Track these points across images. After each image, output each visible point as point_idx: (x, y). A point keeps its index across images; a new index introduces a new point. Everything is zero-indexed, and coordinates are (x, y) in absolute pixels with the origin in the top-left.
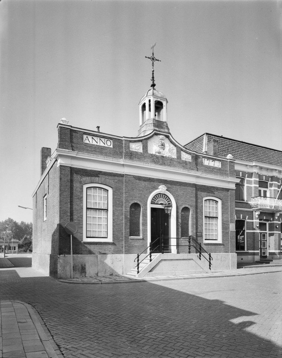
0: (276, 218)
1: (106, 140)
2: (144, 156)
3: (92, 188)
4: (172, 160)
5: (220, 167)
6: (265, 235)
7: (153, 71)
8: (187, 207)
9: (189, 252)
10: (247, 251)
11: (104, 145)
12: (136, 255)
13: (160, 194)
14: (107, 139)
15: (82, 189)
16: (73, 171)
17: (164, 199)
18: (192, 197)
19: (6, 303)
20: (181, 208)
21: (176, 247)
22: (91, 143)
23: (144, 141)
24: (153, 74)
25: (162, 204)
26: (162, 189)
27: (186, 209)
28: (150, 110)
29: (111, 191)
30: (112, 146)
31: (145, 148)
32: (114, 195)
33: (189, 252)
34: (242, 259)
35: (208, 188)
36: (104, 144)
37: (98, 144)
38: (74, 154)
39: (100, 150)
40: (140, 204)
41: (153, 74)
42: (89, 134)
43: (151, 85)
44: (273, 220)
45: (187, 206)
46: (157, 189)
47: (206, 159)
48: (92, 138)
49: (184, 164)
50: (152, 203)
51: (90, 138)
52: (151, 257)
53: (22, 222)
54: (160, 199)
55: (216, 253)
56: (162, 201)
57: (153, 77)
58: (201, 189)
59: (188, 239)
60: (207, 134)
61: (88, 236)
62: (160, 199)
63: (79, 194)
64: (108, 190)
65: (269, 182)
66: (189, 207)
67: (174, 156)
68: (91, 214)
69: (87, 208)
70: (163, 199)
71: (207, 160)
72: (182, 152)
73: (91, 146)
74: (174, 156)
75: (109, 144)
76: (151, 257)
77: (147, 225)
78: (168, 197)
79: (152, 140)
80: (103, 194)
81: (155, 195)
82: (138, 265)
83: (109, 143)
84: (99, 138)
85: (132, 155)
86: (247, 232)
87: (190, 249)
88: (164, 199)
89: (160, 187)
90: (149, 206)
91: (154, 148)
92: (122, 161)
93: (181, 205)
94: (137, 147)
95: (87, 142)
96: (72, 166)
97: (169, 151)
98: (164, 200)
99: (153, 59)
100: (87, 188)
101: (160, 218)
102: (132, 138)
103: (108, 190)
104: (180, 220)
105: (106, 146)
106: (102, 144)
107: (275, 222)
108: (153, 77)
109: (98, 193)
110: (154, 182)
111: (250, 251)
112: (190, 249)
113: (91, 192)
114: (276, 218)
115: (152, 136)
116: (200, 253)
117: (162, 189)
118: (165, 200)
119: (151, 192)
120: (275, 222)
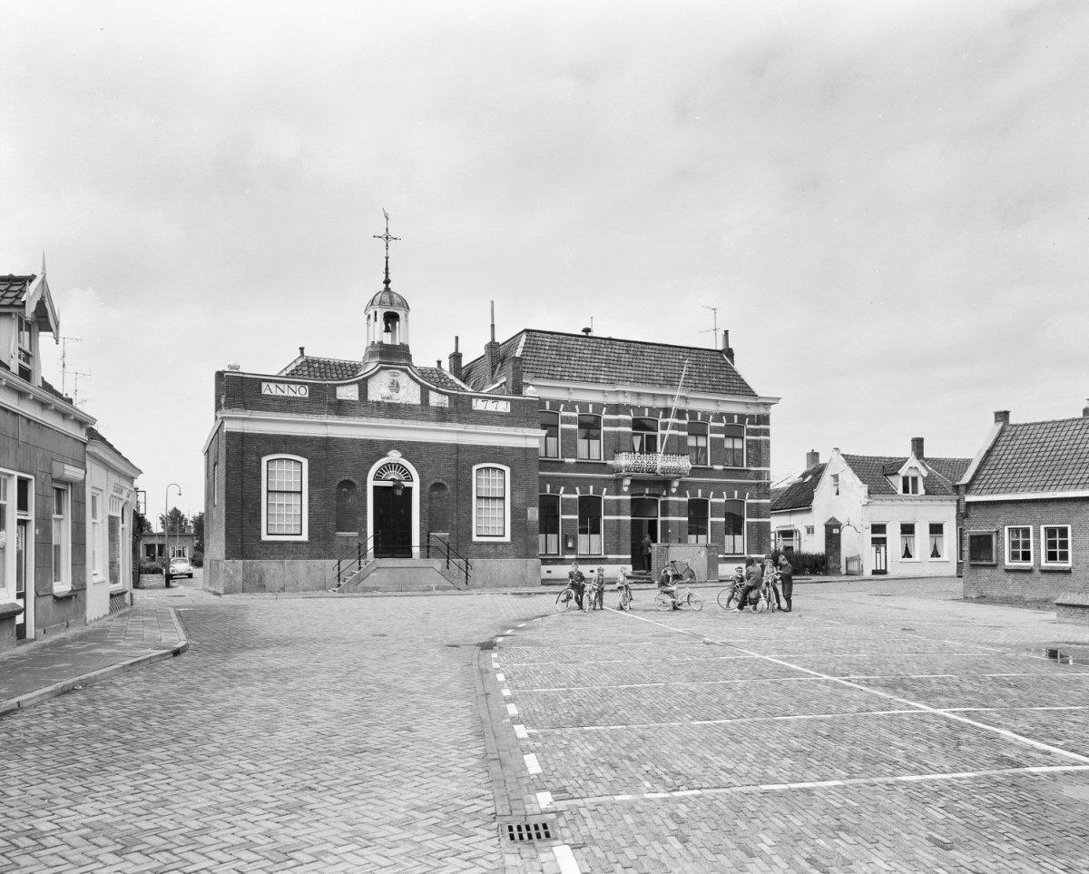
0: (674, 490)
1: (298, 386)
2: (365, 406)
4: (410, 407)
5: (509, 410)
7: (387, 258)
8: (441, 484)
10: (605, 556)
11: (295, 395)
12: (336, 561)
16: (243, 438)
19: (46, 396)
20: (429, 486)
21: (549, 535)
22: (274, 393)
24: (387, 263)
25: (392, 480)
26: (394, 456)
27: (438, 486)
28: (376, 320)
29: (507, 470)
30: (307, 396)
31: (363, 392)
32: (310, 469)
34: (549, 572)
37: (286, 394)
38: (247, 414)
39: (286, 405)
41: (387, 263)
42: (271, 381)
43: (178, 508)
44: (667, 495)
45: (440, 481)
46: (385, 456)
47: (480, 401)
49: (442, 415)
50: (377, 478)
51: (272, 386)
53: (175, 509)
56: (394, 475)
57: (387, 269)
60: (527, 331)
61: (270, 532)
64: (301, 463)
65: (661, 420)
66: (444, 482)
67: (416, 400)
68: (277, 499)
69: (268, 491)
72: (431, 393)
73: (275, 398)
79: (377, 378)
82: (339, 576)
84: (286, 385)
85: (341, 408)
89: (390, 453)
90: (371, 483)
91: (379, 390)
92: (325, 418)
93: (428, 481)
95: (268, 392)
97: (409, 394)
99: (387, 238)
101: (392, 504)
103: (301, 463)
105: (298, 395)
107: (670, 498)
108: (387, 269)
109: (285, 466)
110: (376, 449)
111: (610, 556)
112: (428, 552)
113: (276, 467)
114: (674, 490)
115: (376, 373)
116: (448, 559)
117: (394, 456)
120: (670, 498)
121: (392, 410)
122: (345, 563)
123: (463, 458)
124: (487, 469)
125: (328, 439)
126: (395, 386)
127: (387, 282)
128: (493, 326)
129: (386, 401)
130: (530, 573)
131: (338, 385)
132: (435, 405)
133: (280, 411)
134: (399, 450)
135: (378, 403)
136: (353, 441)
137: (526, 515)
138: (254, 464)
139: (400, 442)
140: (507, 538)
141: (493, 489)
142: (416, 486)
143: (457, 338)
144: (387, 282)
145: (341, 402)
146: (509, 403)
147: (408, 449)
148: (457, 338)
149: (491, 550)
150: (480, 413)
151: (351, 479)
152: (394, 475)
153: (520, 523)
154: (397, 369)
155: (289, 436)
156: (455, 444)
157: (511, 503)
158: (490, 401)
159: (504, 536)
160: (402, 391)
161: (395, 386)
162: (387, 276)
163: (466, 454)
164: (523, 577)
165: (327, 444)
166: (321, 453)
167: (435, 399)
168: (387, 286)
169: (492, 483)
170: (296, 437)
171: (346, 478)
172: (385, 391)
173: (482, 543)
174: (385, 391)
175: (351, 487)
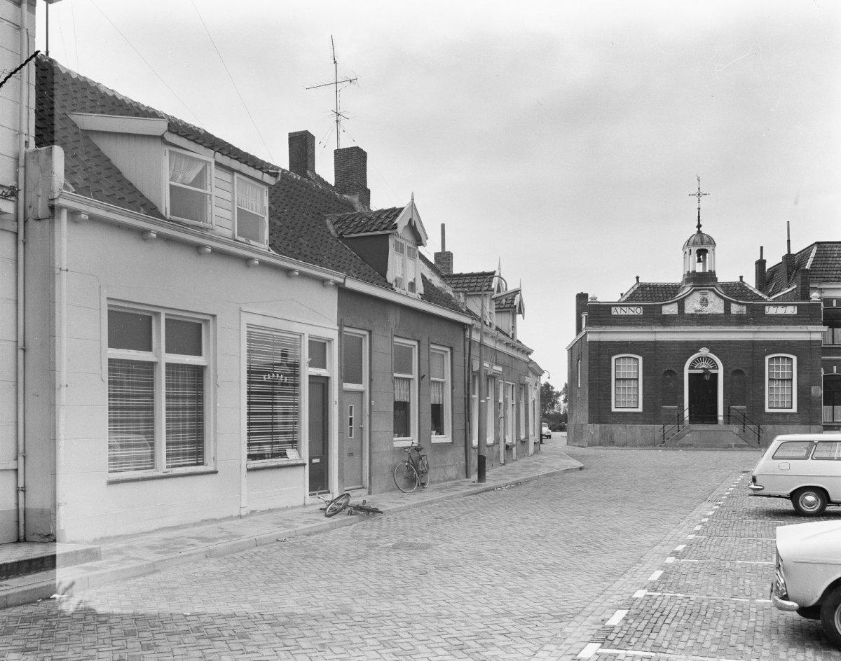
1: (636, 308)
6: (411, 349)
7: (699, 209)
15: (610, 361)
20: (730, 372)
21: (836, 407)
22: (619, 314)
26: (704, 352)
30: (641, 314)
37: (627, 314)
45: (739, 368)
46: (698, 352)
47: (771, 307)
49: (740, 320)
50: (691, 367)
51: (618, 309)
57: (699, 217)
59: (188, 414)
67: (721, 311)
68: (621, 385)
72: (732, 304)
74: (721, 311)
80: (632, 363)
83: (639, 310)
84: (628, 308)
95: (615, 313)
101: (703, 386)
104: (343, 357)
105: (636, 314)
106: (631, 313)
108: (699, 217)
110: (693, 347)
113: (621, 363)
117: (704, 352)
119: (688, 357)
121: (702, 319)
123: (757, 351)
125: (656, 342)
126: (704, 302)
127: (699, 226)
128: (789, 241)
132: (735, 313)
136: (674, 343)
137: (810, 392)
143: (762, 248)
144: (699, 226)
146: (796, 307)
147: (714, 346)
148: (762, 248)
149: (780, 419)
151: (673, 369)
152: (704, 365)
157: (798, 384)
160: (710, 305)
161: (704, 302)
165: (655, 345)
168: (699, 229)
172: (698, 306)
173: (773, 413)
174: (698, 306)
175: (676, 375)
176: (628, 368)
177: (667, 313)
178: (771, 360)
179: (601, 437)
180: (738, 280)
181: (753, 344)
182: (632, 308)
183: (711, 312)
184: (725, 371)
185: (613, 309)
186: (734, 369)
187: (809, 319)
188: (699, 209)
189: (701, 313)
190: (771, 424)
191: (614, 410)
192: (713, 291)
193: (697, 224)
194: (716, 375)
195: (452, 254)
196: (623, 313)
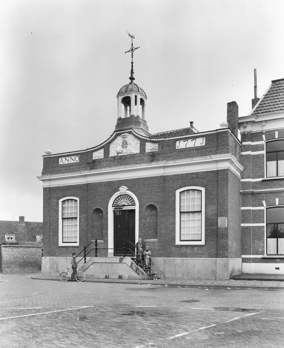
1: (75, 156)
3: (191, 191)
5: (204, 144)
7: (132, 63)
9: (96, 255)
13: (121, 195)
14: (76, 156)
17: (120, 201)
18: (158, 192)
20: (145, 207)
21: (279, 239)
23: (106, 147)
24: (132, 66)
26: (123, 190)
29: (203, 189)
33: (96, 256)
35: (183, 176)
36: (74, 161)
37: (69, 162)
39: (69, 168)
40: (101, 209)
41: (132, 66)
45: (152, 203)
47: (182, 142)
48: (65, 158)
49: (153, 157)
51: (63, 159)
52: (85, 259)
54: (123, 200)
55: (223, 259)
57: (132, 70)
58: (172, 179)
61: (182, 239)
62: (128, 201)
63: (55, 208)
64: (201, 191)
68: (66, 223)
69: (181, 213)
70: (120, 202)
71: (184, 141)
72: (147, 144)
75: (200, 142)
76: (85, 259)
77: (58, 232)
78: (129, 196)
80: (196, 195)
81: (130, 195)
84: (70, 157)
86: (264, 223)
87: (96, 252)
88: (120, 201)
89: (120, 189)
94: (99, 155)
95: (61, 163)
96: (51, 187)
98: (121, 201)
100: (180, 193)
101: (125, 219)
102: (94, 148)
105: (75, 162)
109: (191, 195)
110: (113, 186)
112: (96, 252)
113: (185, 196)
117: (123, 190)
118: (127, 200)
119: (111, 196)
121: (122, 160)
122: (78, 259)
123: (167, 185)
124: (68, 200)
125: (87, 185)
126: (125, 144)
127: (132, 79)
129: (120, 155)
130: (219, 270)
131: (177, 140)
132: (149, 151)
133: (66, 172)
134: (126, 186)
135: (115, 157)
136: (101, 184)
138: (55, 204)
139: (127, 181)
140: (203, 243)
141: (67, 213)
142: (137, 208)
145: (94, 161)
146: (205, 138)
147: (131, 184)
149: (189, 251)
150: (64, 166)
151: (100, 207)
153: (213, 230)
154: (126, 132)
155: (70, 186)
156: (162, 176)
157: (205, 214)
158: (190, 141)
159: (201, 240)
160: (129, 147)
161: (125, 144)
162: (132, 75)
163: (171, 182)
164: (214, 273)
165: (87, 187)
166: (85, 192)
167: (150, 147)
169: (190, 201)
170: (73, 186)
171: (97, 207)
172: (119, 148)
173: (182, 246)
174: (119, 148)
175: (100, 212)
176: (71, 208)
177: (97, 158)
178: (64, 202)
179: (50, 268)
180: (188, 126)
181: (164, 179)
182: (73, 157)
183: (129, 152)
184: (140, 207)
185: (60, 159)
186: (147, 205)
187: (215, 149)
188: (132, 63)
189: (122, 154)
190: (180, 257)
191: (61, 244)
192: (130, 133)
193: (130, 76)
194: (133, 211)
195: (252, 100)
196: (67, 162)
